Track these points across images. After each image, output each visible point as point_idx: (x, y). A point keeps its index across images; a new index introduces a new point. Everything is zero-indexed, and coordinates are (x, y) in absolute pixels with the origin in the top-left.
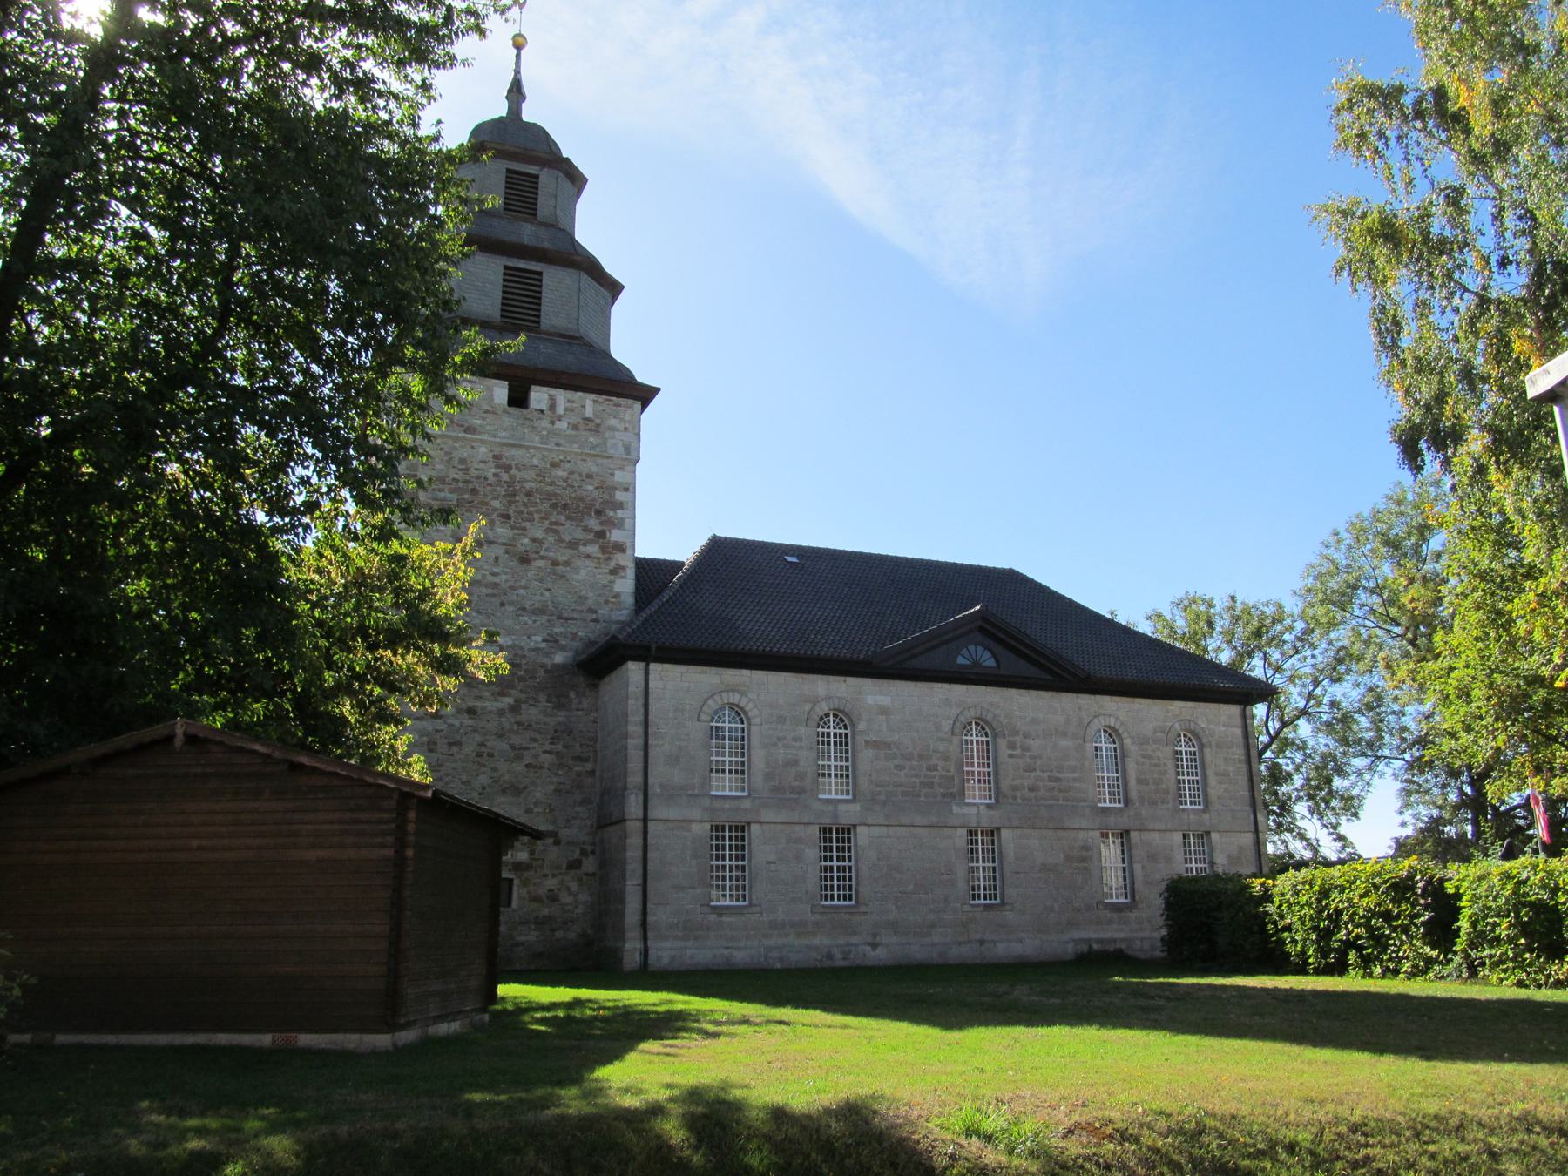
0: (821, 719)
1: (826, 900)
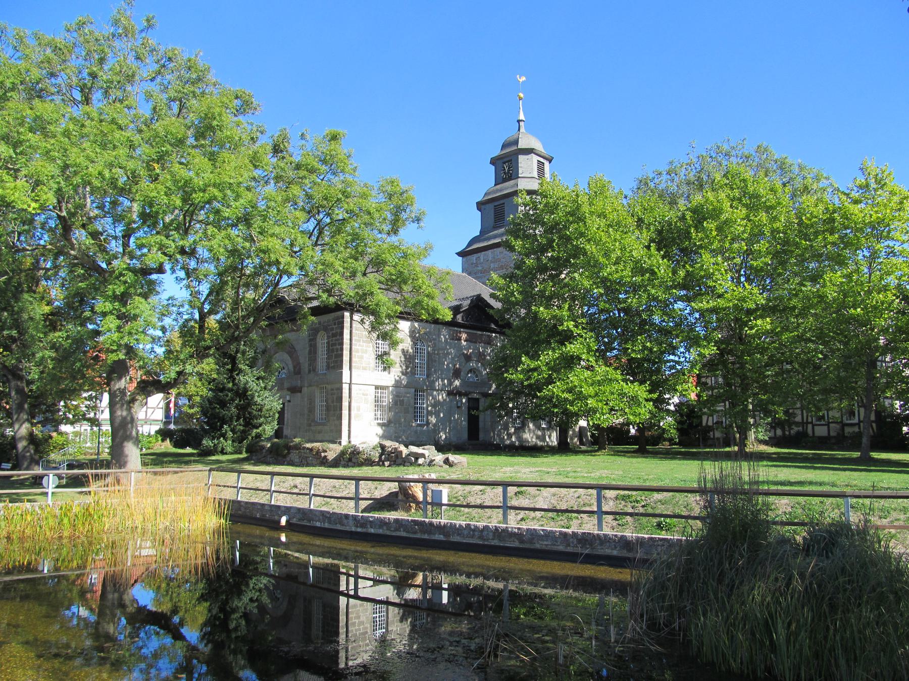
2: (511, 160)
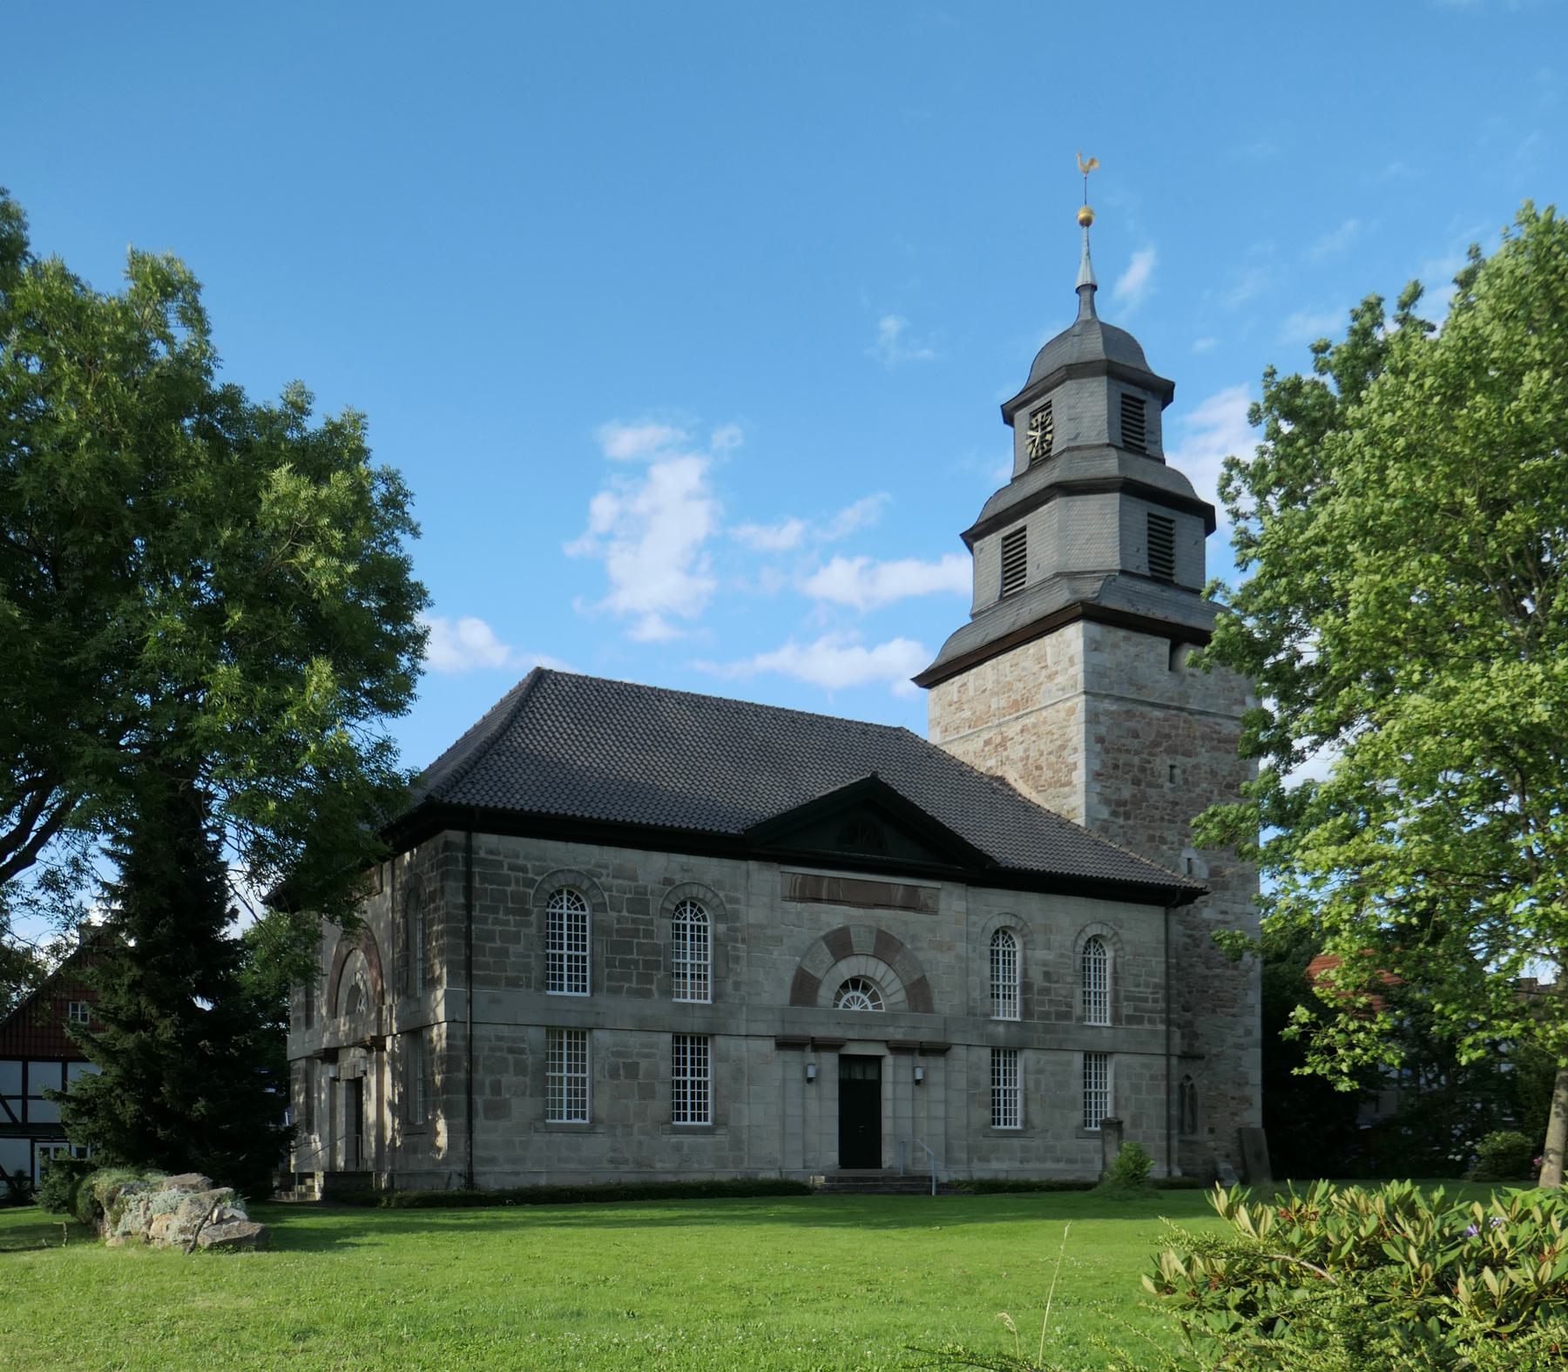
0: (552, 896)
1: (678, 1120)
2: (1048, 405)
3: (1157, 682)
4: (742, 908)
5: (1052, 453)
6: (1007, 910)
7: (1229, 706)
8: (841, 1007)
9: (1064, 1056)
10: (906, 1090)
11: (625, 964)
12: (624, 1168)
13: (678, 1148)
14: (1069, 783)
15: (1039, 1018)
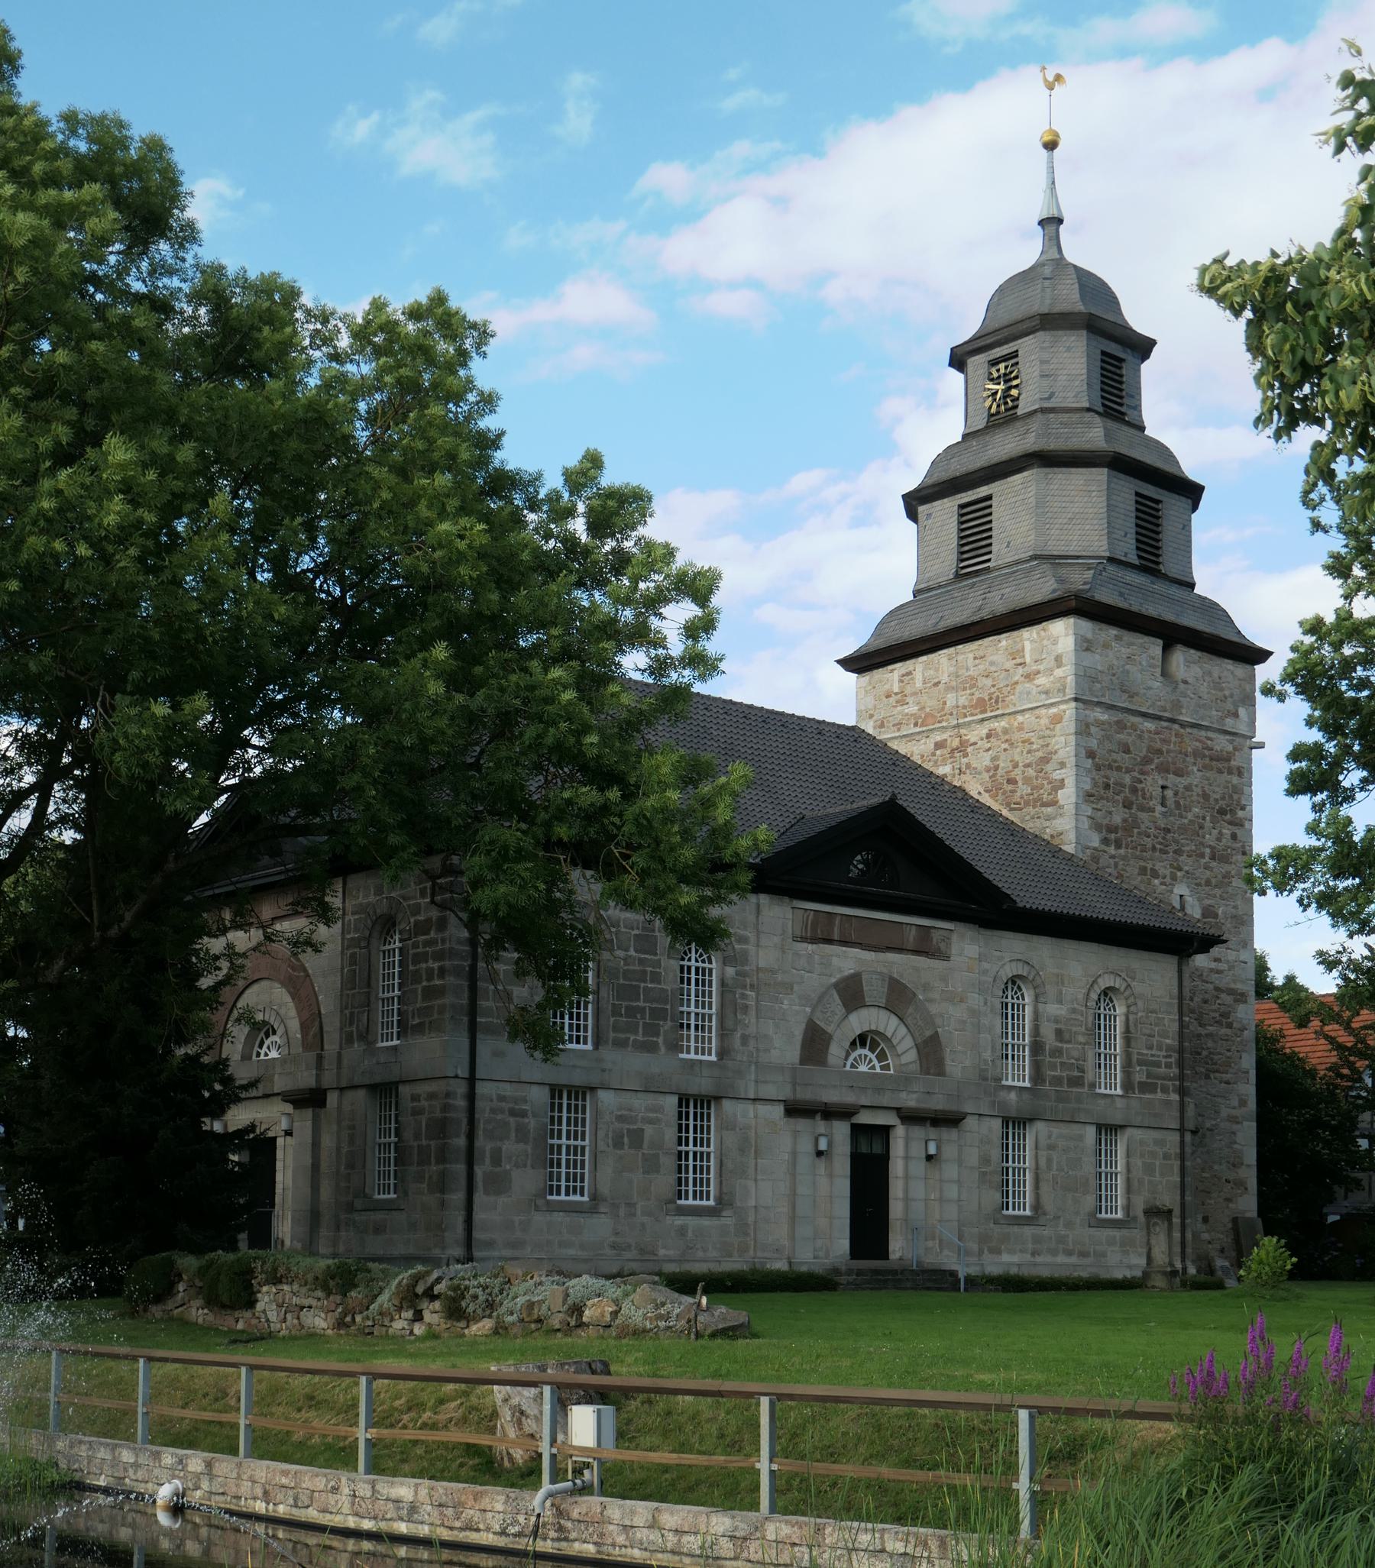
2: (1014, 355)
3: (1150, 688)
4: (751, 948)
5: (1020, 411)
6: (1020, 957)
7: (1222, 718)
8: (848, 1068)
9: (1075, 1129)
10: (919, 1167)
11: (632, 1012)
12: (628, 1255)
13: (682, 1231)
14: (1053, 803)
15: (1051, 1084)
